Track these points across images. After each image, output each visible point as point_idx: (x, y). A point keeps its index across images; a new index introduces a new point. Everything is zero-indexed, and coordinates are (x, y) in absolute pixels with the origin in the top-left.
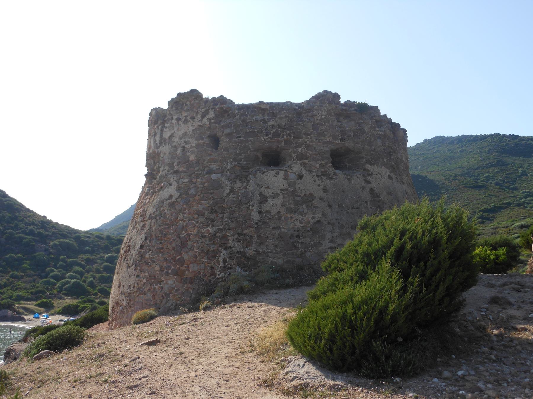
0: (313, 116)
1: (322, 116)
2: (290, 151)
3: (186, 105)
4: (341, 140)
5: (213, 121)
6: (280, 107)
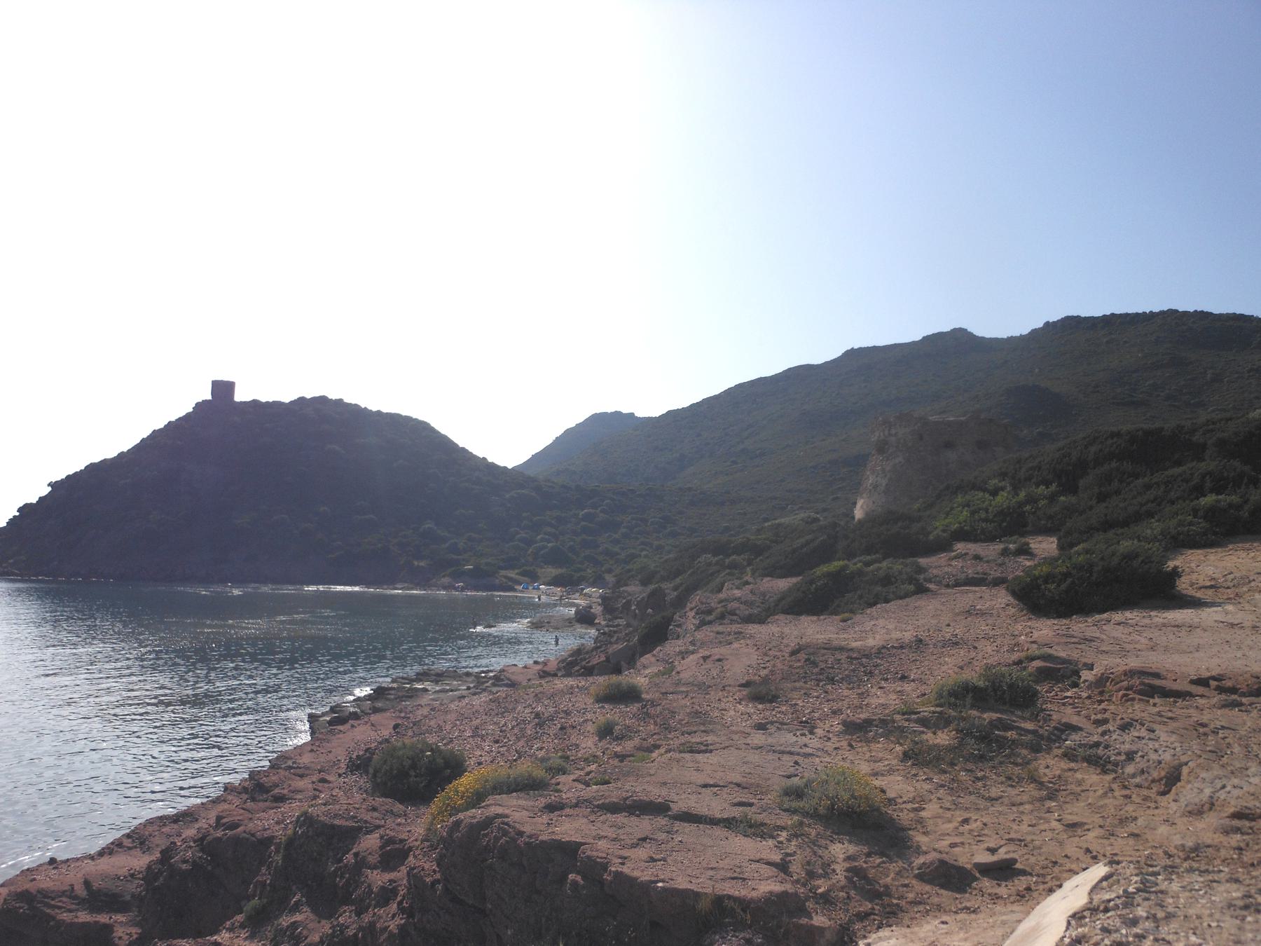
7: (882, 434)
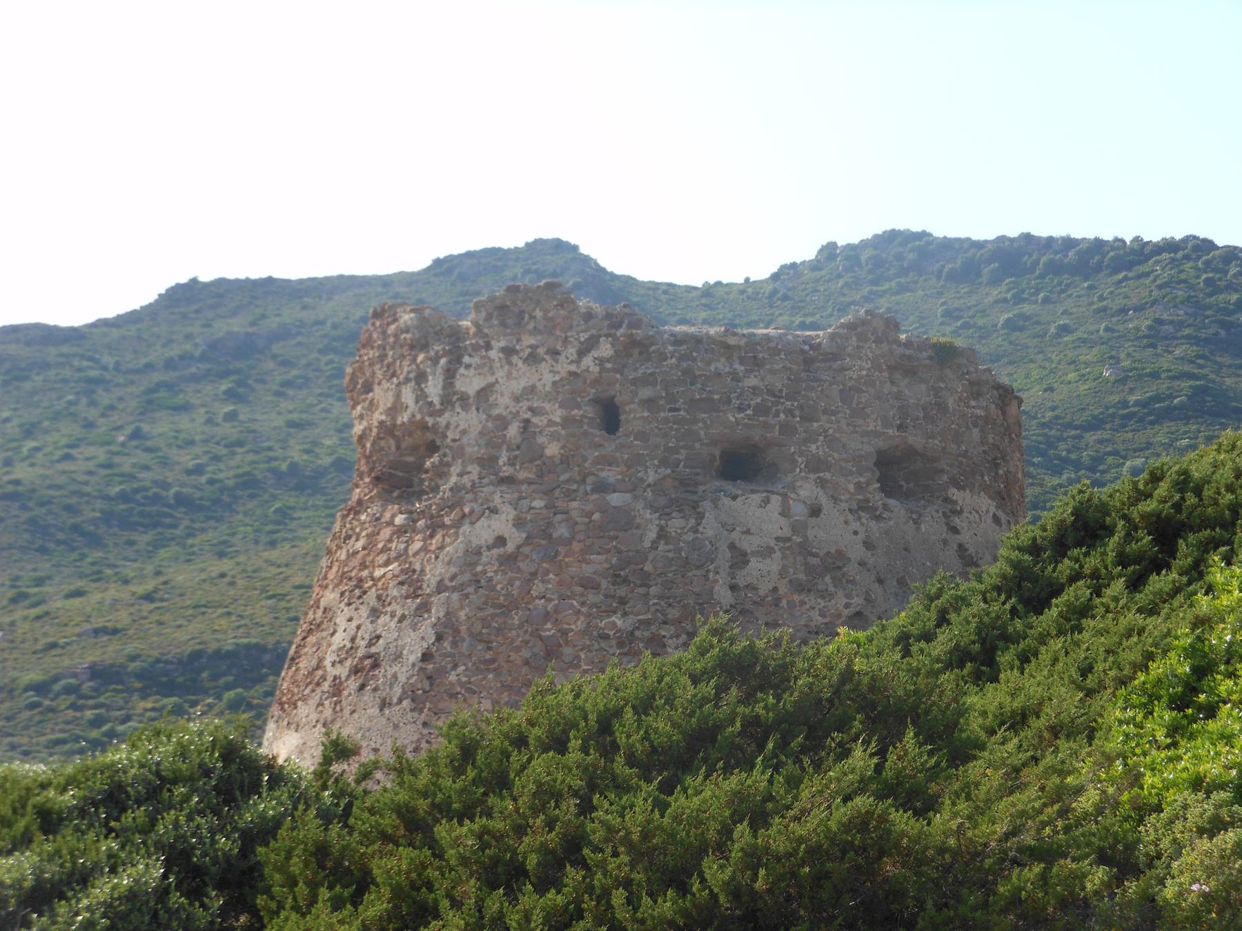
0: (843, 369)
1: (861, 369)
2: (792, 449)
3: (532, 317)
4: (899, 427)
5: (609, 366)
6: (772, 345)
7: (408, 396)
